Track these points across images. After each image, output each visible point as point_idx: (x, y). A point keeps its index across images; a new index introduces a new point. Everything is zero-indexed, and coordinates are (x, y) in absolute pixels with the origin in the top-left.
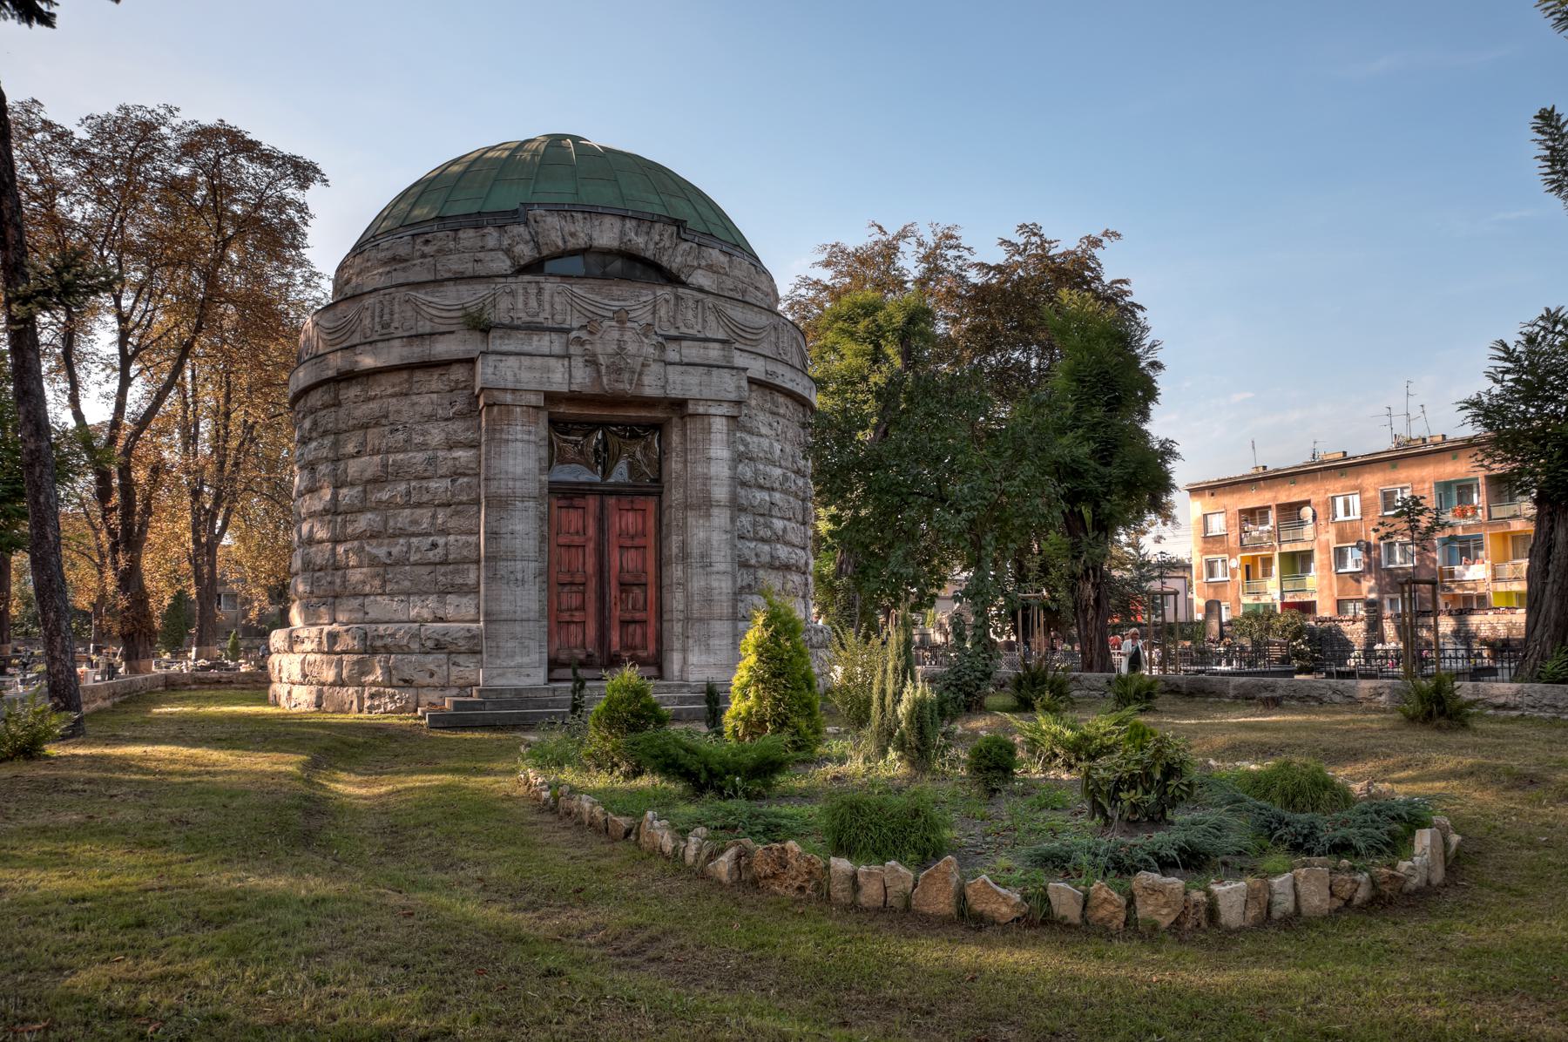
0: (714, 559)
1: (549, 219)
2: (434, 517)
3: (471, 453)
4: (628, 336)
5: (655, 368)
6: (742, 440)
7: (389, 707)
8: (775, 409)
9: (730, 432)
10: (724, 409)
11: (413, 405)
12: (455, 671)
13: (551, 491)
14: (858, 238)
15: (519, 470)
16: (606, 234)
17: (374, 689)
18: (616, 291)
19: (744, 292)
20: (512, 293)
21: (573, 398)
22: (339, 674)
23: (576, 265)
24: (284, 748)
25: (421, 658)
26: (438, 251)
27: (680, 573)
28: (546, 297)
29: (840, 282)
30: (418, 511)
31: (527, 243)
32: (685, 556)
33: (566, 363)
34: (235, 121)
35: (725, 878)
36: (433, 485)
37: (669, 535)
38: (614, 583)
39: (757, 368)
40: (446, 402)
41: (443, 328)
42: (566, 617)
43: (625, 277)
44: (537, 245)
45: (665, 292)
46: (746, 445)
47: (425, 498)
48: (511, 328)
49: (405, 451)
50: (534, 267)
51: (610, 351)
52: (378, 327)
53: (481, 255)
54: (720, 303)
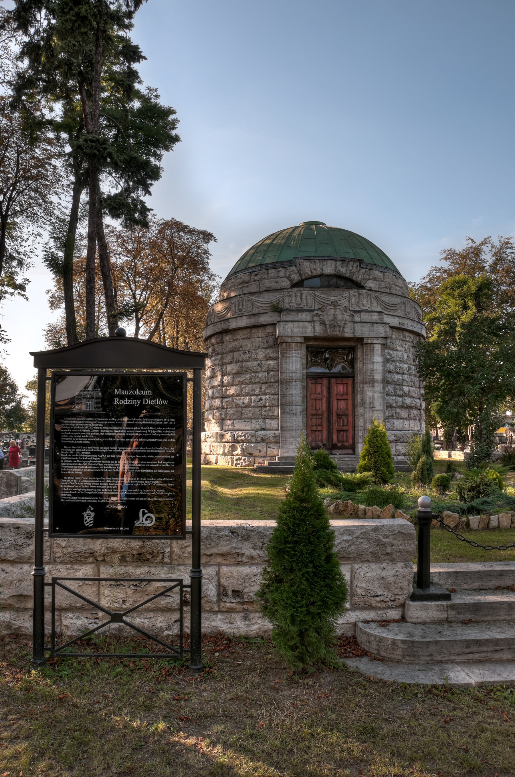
0: (376, 404)
1: (305, 263)
2: (261, 388)
3: (275, 362)
4: (338, 312)
5: (350, 325)
6: (389, 353)
7: (243, 464)
8: (404, 339)
9: (383, 350)
10: (380, 341)
11: (252, 342)
12: (269, 450)
13: (307, 377)
14: (461, 247)
15: (294, 369)
16: (329, 268)
17: (237, 457)
18: (333, 293)
19: (390, 288)
20: (290, 296)
21: (316, 338)
22: (224, 451)
23: (317, 282)
24: (251, 252)
25: (256, 444)
26: (261, 278)
27: (361, 410)
28: (304, 296)
29: (452, 268)
30: (255, 386)
31: (296, 274)
32: (363, 403)
33: (312, 324)
34: (178, 219)
35: (332, 512)
36: (260, 375)
37: (357, 394)
38: (334, 414)
39: (395, 322)
40: (265, 341)
41: (263, 311)
42: (314, 428)
43: (337, 287)
44: (300, 275)
45: (354, 292)
46: (391, 355)
47: (257, 380)
48: (289, 311)
49: (249, 361)
50: (299, 284)
51: (330, 318)
52: (237, 311)
53: (278, 280)
54: (378, 295)
